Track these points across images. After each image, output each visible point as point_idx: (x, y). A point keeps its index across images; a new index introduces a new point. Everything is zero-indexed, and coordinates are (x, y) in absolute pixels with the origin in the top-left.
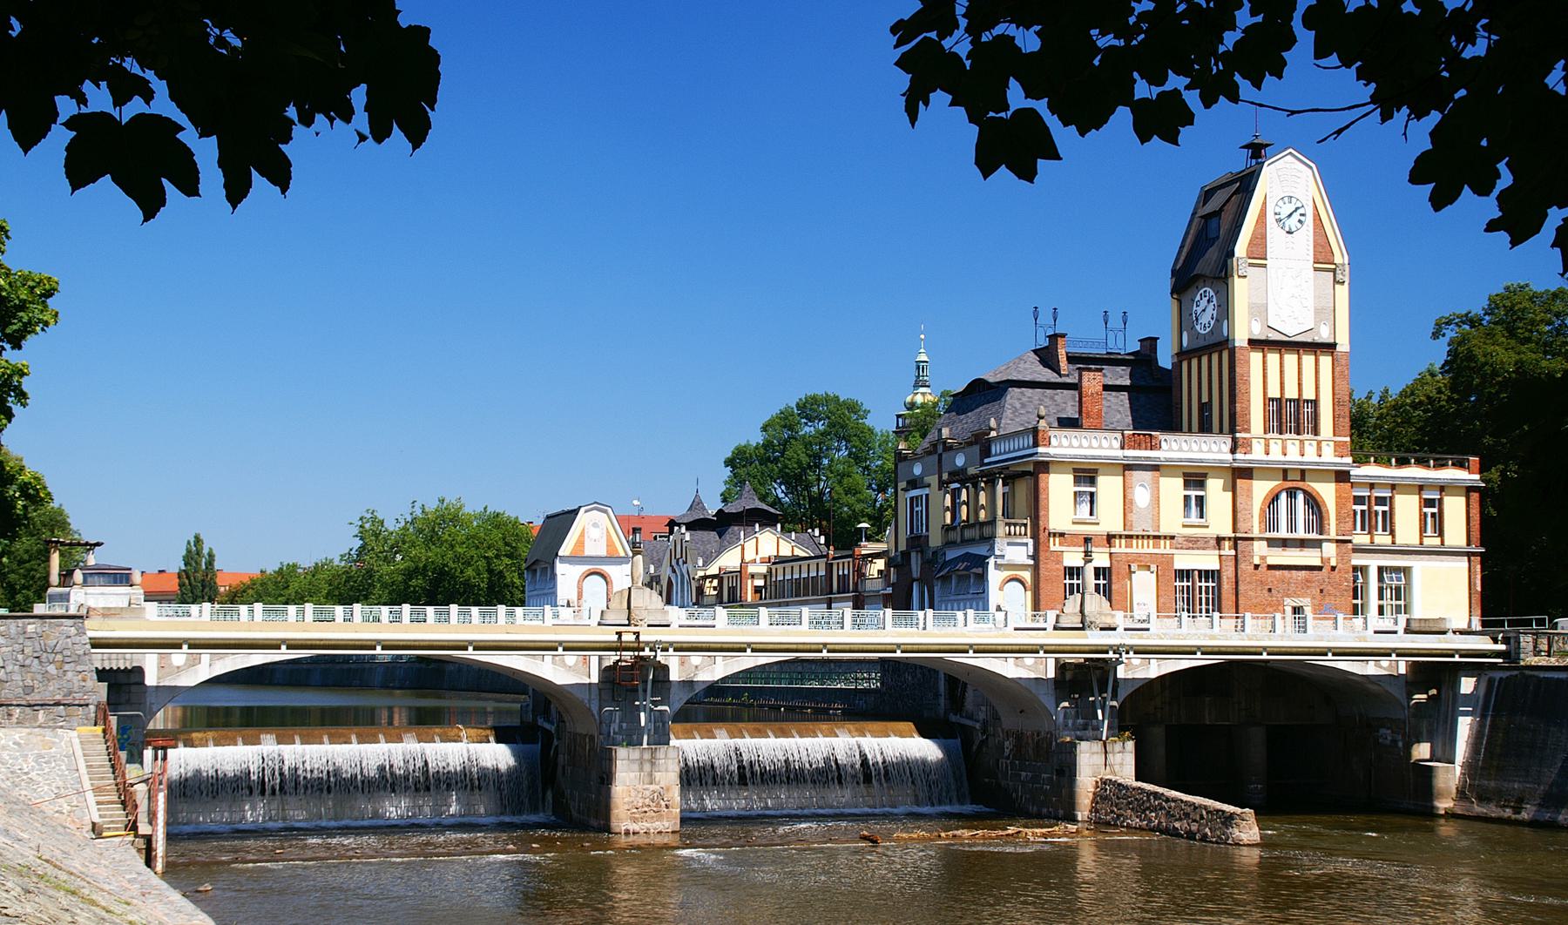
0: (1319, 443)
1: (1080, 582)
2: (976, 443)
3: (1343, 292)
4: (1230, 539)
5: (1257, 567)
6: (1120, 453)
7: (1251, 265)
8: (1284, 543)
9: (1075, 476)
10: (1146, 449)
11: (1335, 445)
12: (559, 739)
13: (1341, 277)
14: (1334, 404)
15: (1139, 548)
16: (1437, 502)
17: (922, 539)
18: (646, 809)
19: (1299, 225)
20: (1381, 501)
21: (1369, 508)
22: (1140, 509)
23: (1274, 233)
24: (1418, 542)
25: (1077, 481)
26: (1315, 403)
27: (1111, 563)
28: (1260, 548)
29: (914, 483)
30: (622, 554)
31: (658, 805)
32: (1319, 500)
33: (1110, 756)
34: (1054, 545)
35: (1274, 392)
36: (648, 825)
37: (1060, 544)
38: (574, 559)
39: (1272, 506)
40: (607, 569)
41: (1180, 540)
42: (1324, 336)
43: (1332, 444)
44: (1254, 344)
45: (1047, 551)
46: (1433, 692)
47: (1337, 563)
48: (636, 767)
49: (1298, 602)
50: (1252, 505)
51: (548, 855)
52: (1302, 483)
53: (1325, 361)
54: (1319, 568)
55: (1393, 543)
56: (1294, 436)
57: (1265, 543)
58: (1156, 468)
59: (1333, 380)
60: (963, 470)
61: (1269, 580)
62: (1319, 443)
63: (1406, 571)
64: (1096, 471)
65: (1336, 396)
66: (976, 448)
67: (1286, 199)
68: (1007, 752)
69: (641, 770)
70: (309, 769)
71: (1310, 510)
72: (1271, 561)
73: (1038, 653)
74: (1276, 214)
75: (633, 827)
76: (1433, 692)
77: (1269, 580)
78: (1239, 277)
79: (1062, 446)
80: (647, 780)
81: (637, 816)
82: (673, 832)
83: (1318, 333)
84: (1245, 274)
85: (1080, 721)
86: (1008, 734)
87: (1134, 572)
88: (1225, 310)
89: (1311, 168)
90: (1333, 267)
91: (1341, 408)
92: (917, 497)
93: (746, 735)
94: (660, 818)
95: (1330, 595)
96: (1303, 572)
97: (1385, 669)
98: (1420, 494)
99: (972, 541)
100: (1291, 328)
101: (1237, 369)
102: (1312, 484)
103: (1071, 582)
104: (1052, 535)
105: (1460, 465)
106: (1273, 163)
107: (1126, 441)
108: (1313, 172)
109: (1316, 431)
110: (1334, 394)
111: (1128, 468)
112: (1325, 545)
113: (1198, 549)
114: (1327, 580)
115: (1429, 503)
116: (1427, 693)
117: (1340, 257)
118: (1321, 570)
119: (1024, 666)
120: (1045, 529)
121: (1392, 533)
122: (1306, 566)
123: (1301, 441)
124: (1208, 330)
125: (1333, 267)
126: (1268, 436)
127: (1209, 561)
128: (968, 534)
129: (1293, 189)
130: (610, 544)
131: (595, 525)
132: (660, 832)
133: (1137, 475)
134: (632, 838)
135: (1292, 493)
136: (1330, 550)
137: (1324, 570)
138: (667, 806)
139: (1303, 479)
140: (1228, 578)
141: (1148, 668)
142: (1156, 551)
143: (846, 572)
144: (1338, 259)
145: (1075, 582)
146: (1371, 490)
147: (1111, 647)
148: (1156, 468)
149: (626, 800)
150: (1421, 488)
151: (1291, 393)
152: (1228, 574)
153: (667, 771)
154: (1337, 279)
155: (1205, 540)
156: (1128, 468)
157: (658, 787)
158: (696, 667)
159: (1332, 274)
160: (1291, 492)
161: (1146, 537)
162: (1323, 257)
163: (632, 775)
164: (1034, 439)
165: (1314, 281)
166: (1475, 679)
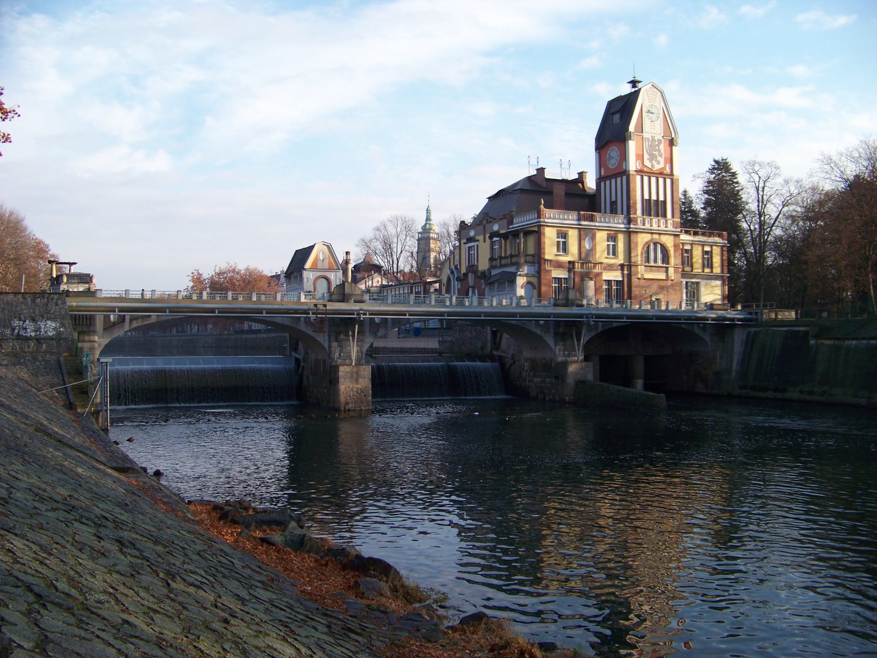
2: (505, 218)
12: (304, 362)
16: (710, 253)
17: (475, 267)
26: (665, 202)
29: (470, 240)
60: (497, 232)
66: (505, 221)
68: (526, 368)
70: (233, 621)
85: (566, 353)
86: (527, 360)
88: (624, 157)
92: (471, 247)
93: (477, 360)
99: (506, 265)
101: (631, 185)
105: (720, 236)
109: (665, 216)
115: (707, 253)
124: (615, 166)
128: (503, 262)
143: (419, 290)
164: (538, 214)
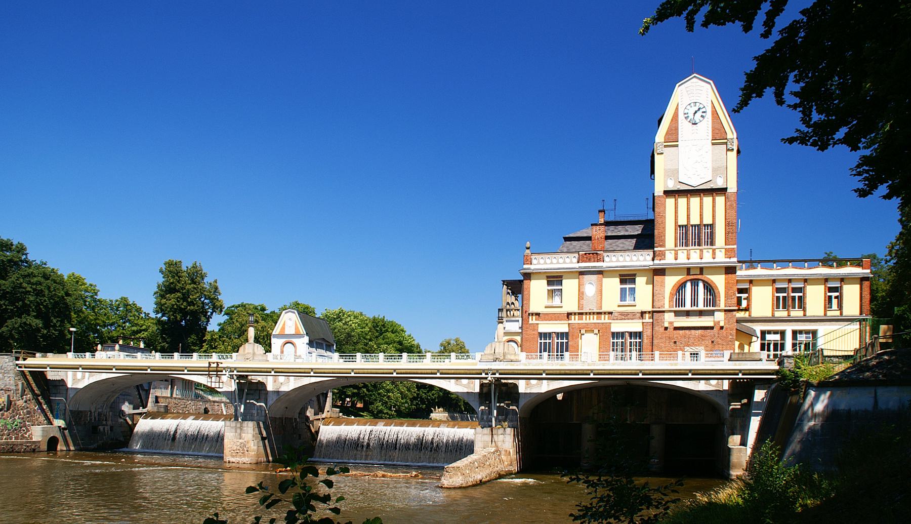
0: (714, 250)
1: (551, 341)
3: (733, 155)
4: (649, 312)
5: (666, 329)
6: (577, 265)
7: (665, 146)
8: (688, 314)
9: (548, 281)
10: (594, 261)
11: (725, 251)
13: (731, 146)
14: (725, 225)
15: (586, 320)
18: (238, 451)
19: (702, 119)
20: (795, 290)
21: (788, 294)
22: (589, 297)
23: (684, 125)
24: (823, 314)
25: (549, 283)
26: (712, 226)
27: (569, 329)
28: (669, 318)
30: (302, 333)
31: (243, 450)
32: (713, 285)
33: (495, 436)
34: (532, 320)
35: (682, 221)
36: (239, 459)
37: (536, 320)
38: (279, 336)
39: (681, 291)
40: (294, 340)
41: (616, 315)
42: (720, 184)
43: (723, 250)
44: (668, 193)
45: (527, 324)
46: (745, 401)
47: (725, 324)
48: (234, 431)
49: (694, 349)
50: (664, 291)
51: (507, 499)
52: (701, 276)
53: (720, 200)
54: (712, 328)
55: (805, 315)
56: (697, 247)
57: (673, 314)
58: (600, 273)
59: (725, 210)
61: (675, 336)
62: (714, 250)
63: (814, 333)
64: (561, 277)
65: (727, 221)
67: (692, 105)
69: (236, 432)
71: (709, 293)
72: (676, 325)
73: (436, 374)
74: (685, 114)
75: (232, 460)
76: (745, 401)
77: (675, 336)
78: (658, 154)
79: (540, 264)
80: (239, 437)
81: (234, 454)
82: (250, 463)
83: (716, 182)
84: (662, 152)
87: (583, 334)
89: (709, 83)
90: (726, 141)
91: (730, 227)
94: (244, 456)
95: (719, 344)
96: (700, 331)
97: (713, 386)
98: (825, 284)
100: (695, 182)
102: (709, 277)
103: (545, 341)
104: (531, 315)
106: (682, 84)
107: (580, 258)
108: (711, 86)
110: (726, 219)
111: (582, 273)
112: (716, 313)
113: (628, 319)
114: (717, 335)
115: (831, 290)
116: (741, 402)
117: (731, 134)
118: (713, 329)
119: (461, 385)
120: (526, 311)
121: (804, 310)
122: (701, 327)
123: (700, 250)
125: (726, 141)
126: (676, 249)
127: (635, 326)
129: (698, 98)
130: (297, 328)
131: (290, 319)
132: (244, 463)
133: (587, 278)
134: (231, 464)
135: (695, 282)
136: (720, 317)
137: (714, 329)
138: (247, 451)
139: (701, 273)
140: (647, 336)
141: (541, 386)
142: (598, 321)
144: (729, 136)
145: (548, 341)
146: (789, 283)
147: (484, 370)
148: (600, 273)
149: (229, 446)
150: (826, 280)
151: (695, 220)
152: (647, 334)
153: (247, 433)
154: (728, 148)
155: (634, 314)
156: (582, 273)
157: (243, 441)
158: (281, 383)
159: (725, 145)
160: (695, 282)
161: (592, 314)
162: (718, 137)
163: (232, 434)
165: (712, 151)
166: (765, 391)
